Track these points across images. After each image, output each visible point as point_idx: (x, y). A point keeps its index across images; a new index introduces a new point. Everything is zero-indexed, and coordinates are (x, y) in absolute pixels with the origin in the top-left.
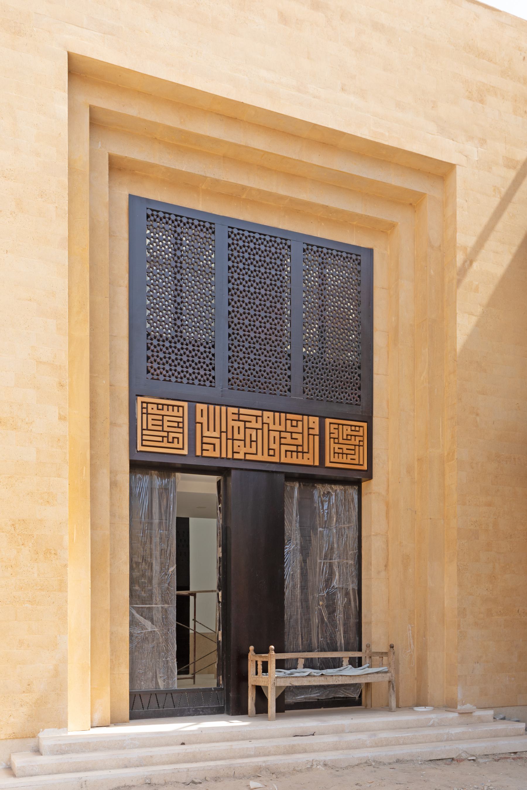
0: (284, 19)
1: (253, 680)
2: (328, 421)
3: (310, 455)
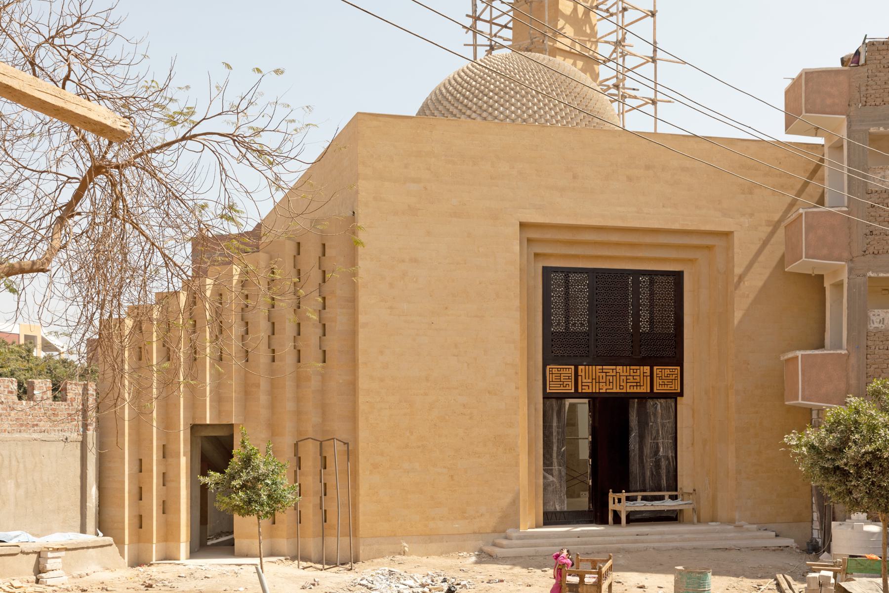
0: (630, 179)
1: (611, 506)
2: (655, 368)
3: (645, 387)
